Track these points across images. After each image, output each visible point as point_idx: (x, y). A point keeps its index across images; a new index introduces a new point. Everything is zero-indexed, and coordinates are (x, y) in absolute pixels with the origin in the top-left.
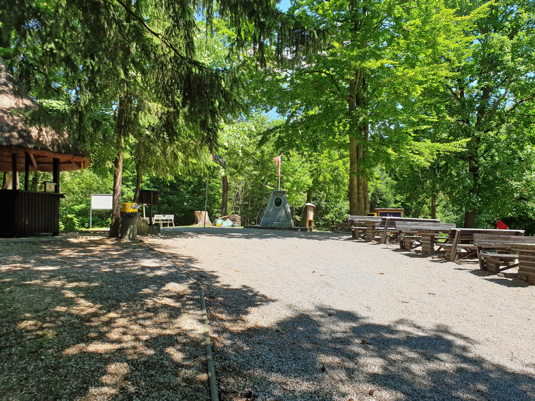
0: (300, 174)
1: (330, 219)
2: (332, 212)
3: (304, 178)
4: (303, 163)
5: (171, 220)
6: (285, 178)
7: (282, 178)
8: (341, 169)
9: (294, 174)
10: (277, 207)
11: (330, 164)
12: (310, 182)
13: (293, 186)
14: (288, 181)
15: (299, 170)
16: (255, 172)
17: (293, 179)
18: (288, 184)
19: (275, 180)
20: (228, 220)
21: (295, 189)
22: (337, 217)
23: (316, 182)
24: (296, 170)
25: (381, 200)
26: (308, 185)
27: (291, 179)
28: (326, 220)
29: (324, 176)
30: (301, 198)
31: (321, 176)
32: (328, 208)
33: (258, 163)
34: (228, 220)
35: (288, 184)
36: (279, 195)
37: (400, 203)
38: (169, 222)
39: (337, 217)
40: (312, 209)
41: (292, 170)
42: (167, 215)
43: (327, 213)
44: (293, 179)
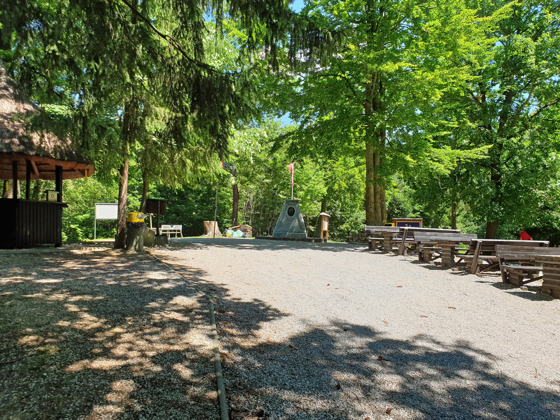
0: (314, 182)
1: (346, 230)
2: (348, 222)
3: (318, 186)
4: (317, 170)
5: (179, 231)
6: (298, 186)
7: (295, 186)
8: (356, 177)
9: (307, 182)
10: (290, 217)
11: (346, 172)
12: (324, 190)
13: (306, 195)
14: (301, 189)
15: (313, 178)
16: (267, 181)
17: (306, 188)
18: (301, 193)
19: (288, 188)
20: (239, 231)
21: (309, 198)
22: (352, 228)
23: (330, 190)
24: (310, 179)
25: (399, 209)
26: (323, 194)
27: (305, 188)
28: (341, 231)
29: (339, 185)
30: (315, 208)
31: (336, 184)
32: (343, 217)
33: (270, 171)
34: (239, 231)
35: (302, 192)
36: (292, 205)
37: (418, 213)
38: (177, 232)
39: (352, 228)
40: (326, 219)
41: (305, 178)
42: (175, 226)
43: (343, 223)
44: (306, 188)
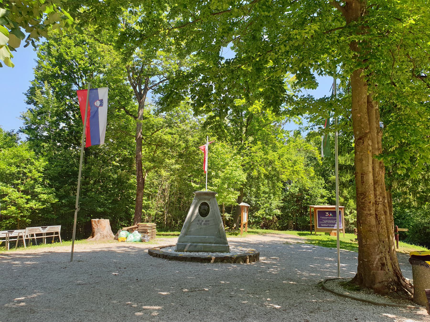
0: (231, 168)
1: (261, 216)
2: (262, 209)
3: (237, 173)
4: (235, 155)
5: (57, 233)
6: (213, 173)
7: (209, 173)
8: (276, 163)
9: (224, 169)
10: (203, 218)
11: (265, 157)
12: (244, 177)
13: (223, 183)
14: (217, 176)
15: (231, 163)
16: (177, 166)
17: (223, 174)
18: (216, 181)
19: (202, 175)
20: (136, 232)
21: (226, 186)
22: (267, 214)
23: (249, 177)
24: (227, 164)
25: (308, 195)
26: (242, 182)
27: (221, 174)
28: (256, 217)
29: (259, 171)
30: (232, 198)
31: (255, 170)
32: (258, 204)
33: (181, 155)
34: (136, 232)
35: (218, 180)
36: (205, 199)
37: (326, 198)
38: (54, 236)
39: (267, 214)
40: (246, 209)
41: (222, 163)
42: (48, 227)
43: (258, 209)
44: (223, 174)
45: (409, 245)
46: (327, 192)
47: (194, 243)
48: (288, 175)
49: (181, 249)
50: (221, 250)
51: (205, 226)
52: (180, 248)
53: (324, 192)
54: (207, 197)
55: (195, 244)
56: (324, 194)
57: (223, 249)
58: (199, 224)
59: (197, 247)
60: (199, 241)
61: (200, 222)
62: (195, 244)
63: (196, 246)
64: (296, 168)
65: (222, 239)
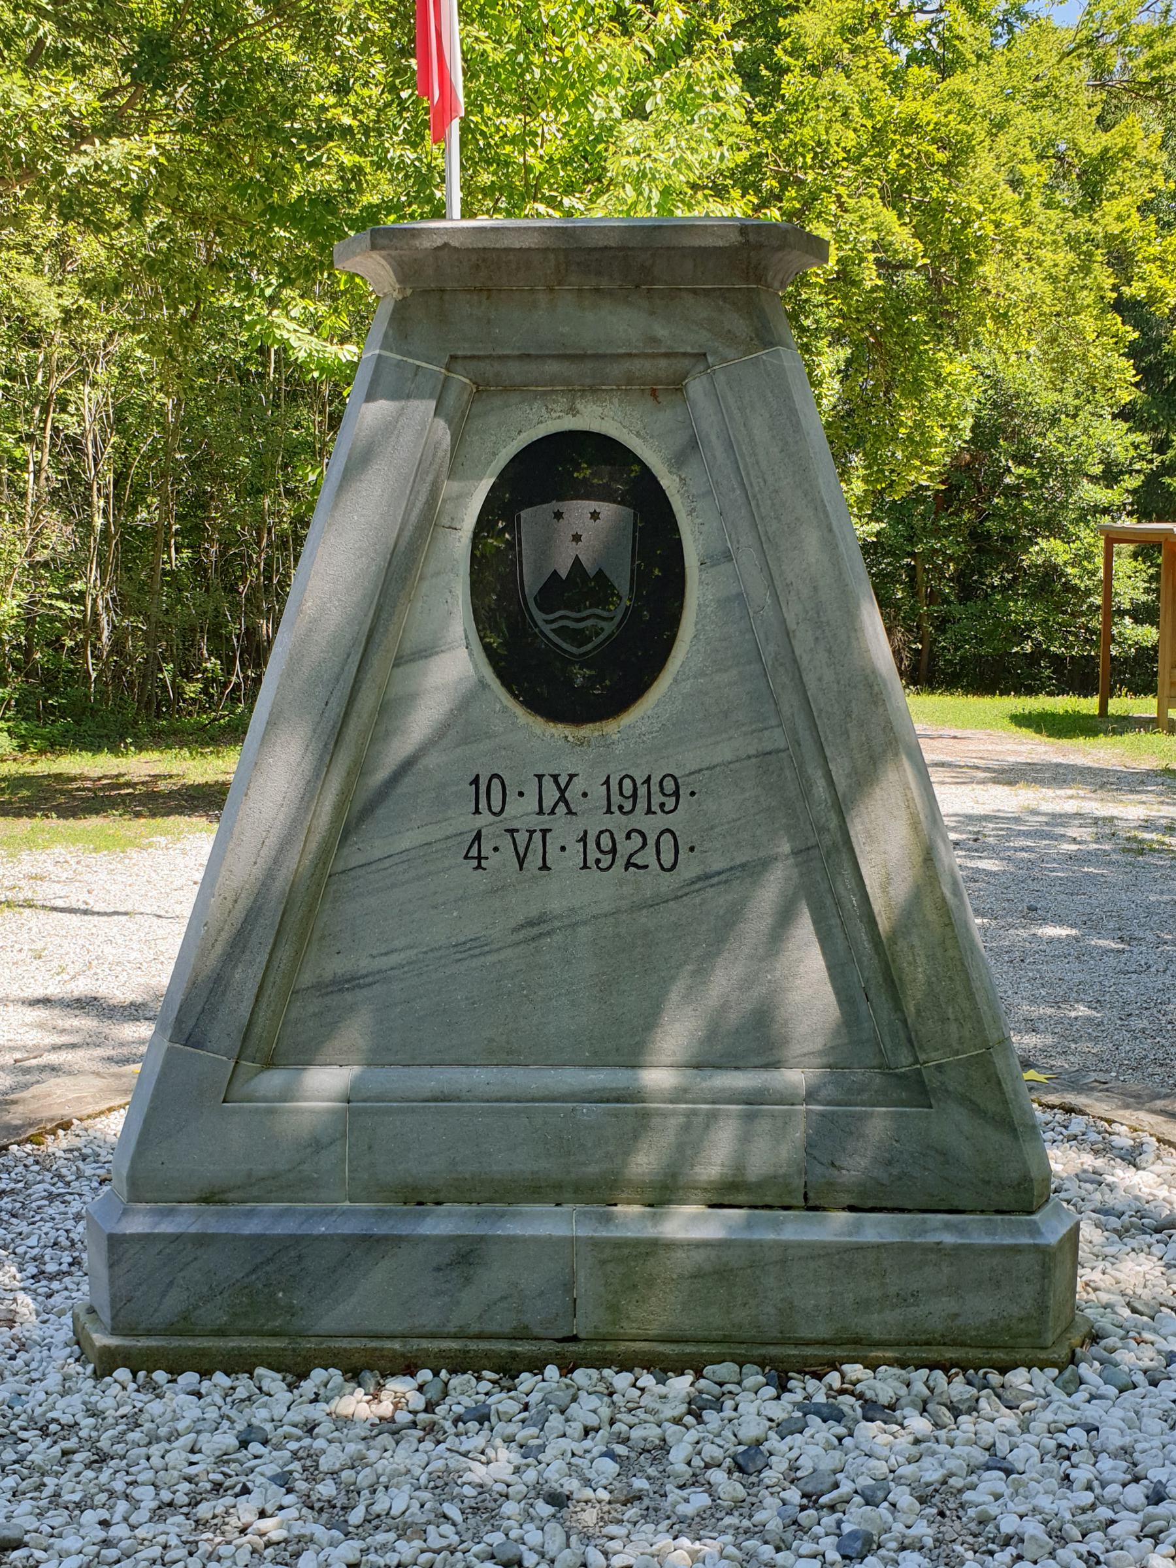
36: (590, 371)
45: (493, 676)
46: (1138, 437)
47: (419, 1197)
48: (1062, 272)
49: (182, 1326)
50: (936, 1312)
51: (603, 890)
52: (173, 1303)
53: (1119, 440)
54: (620, 325)
55: (442, 1223)
56: (1120, 453)
57: (981, 1308)
58: (501, 860)
59: (494, 1278)
60: (525, 1163)
61: (522, 811)
62: (442, 1223)
63: (465, 1256)
64: (1119, 218)
65: (951, 1126)
